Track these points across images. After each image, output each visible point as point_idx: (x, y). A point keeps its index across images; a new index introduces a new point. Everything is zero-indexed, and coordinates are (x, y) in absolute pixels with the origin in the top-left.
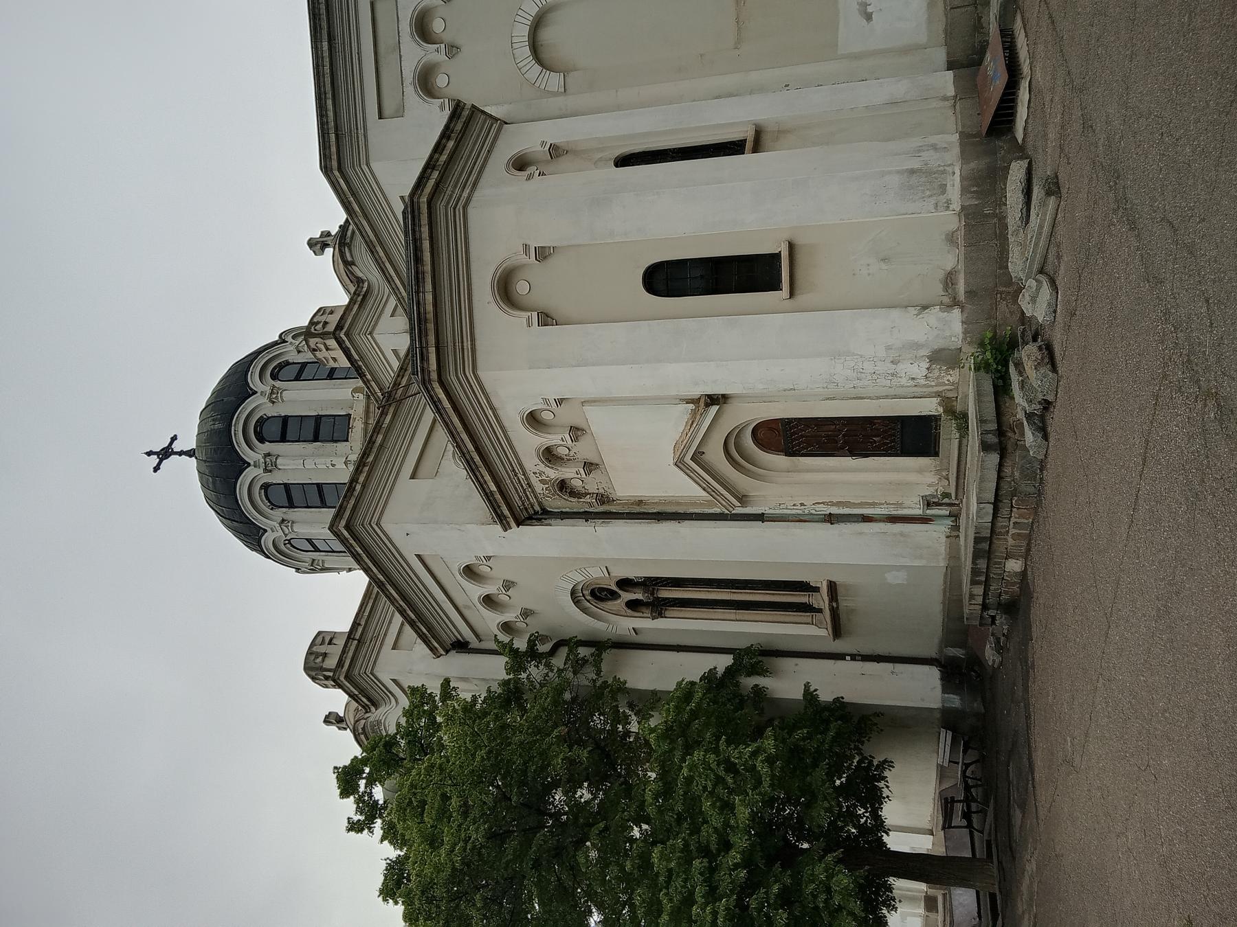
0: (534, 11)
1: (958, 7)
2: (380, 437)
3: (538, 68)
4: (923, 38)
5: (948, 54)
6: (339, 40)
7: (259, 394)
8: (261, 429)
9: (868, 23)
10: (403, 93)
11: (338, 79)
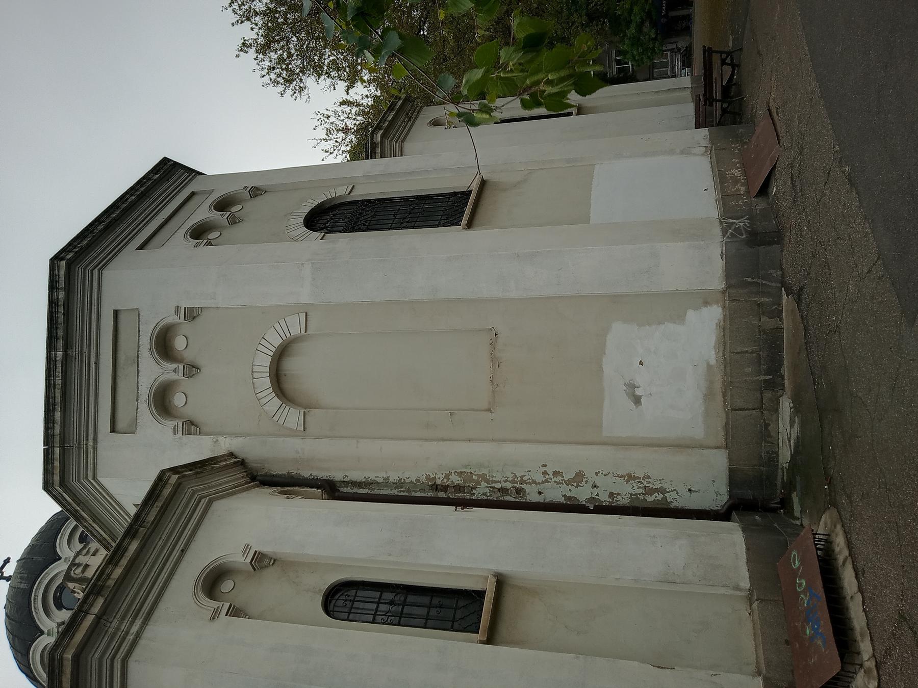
0: (277, 342)
1: (741, 409)
3: (277, 402)
4: (698, 432)
5: (730, 460)
7: (62, 560)
8: (61, 594)
9: (637, 407)
10: (137, 409)
11: (71, 383)
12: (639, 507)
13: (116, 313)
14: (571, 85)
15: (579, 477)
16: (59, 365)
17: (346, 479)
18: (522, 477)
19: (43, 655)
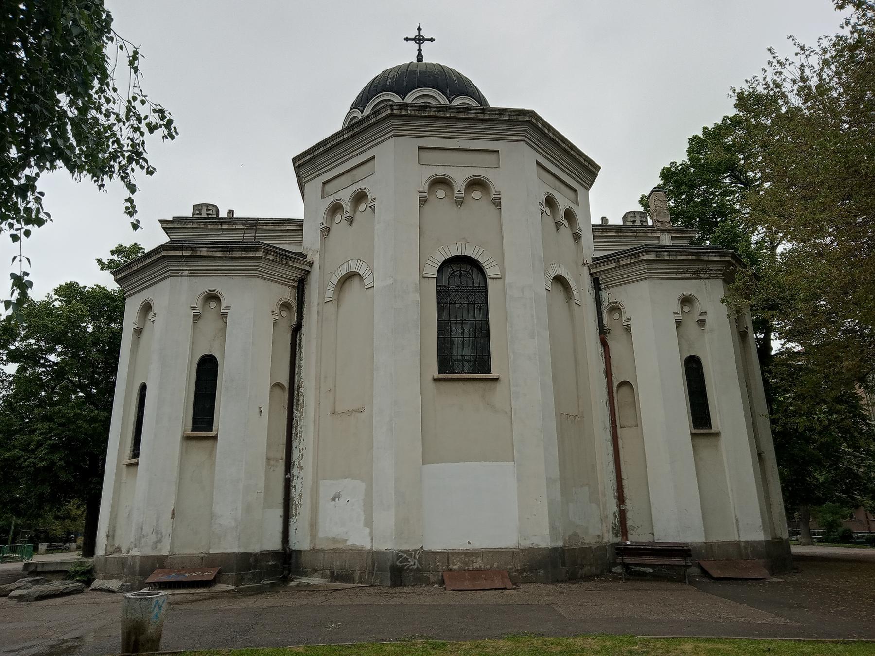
2: (226, 227)
4: (321, 535)
6: (354, 142)
12: (782, 487)
13: (373, 158)
14: (862, 409)
15: (301, 468)
16: (342, 138)
17: (302, 335)
18: (301, 436)
19: (353, 119)
